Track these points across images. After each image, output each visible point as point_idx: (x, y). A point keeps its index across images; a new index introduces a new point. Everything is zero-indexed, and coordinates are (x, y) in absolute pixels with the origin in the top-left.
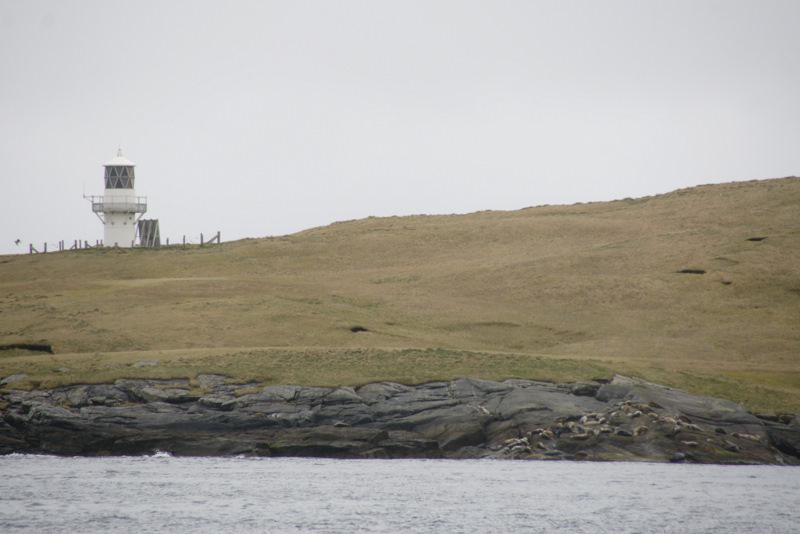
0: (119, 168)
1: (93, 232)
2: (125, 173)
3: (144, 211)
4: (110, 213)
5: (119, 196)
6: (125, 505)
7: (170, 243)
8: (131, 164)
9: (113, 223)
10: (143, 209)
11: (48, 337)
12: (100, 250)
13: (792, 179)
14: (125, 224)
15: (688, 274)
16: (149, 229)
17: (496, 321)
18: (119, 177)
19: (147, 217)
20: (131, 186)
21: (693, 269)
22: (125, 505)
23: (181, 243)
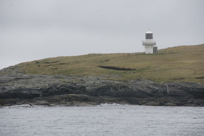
0: (150, 34)
1: (142, 49)
2: (151, 35)
3: (156, 45)
4: (146, 45)
5: (149, 41)
6: (187, 98)
7: (150, 53)
8: (152, 33)
9: (149, 48)
10: (155, 44)
11: (23, 108)
12: (144, 54)
13: (203, 45)
14: (149, 48)
15: (127, 67)
16: (155, 49)
17: (12, 109)
18: (149, 36)
19: (156, 46)
20: (152, 39)
21: (122, 67)
22: (187, 98)
23: (149, 53)
